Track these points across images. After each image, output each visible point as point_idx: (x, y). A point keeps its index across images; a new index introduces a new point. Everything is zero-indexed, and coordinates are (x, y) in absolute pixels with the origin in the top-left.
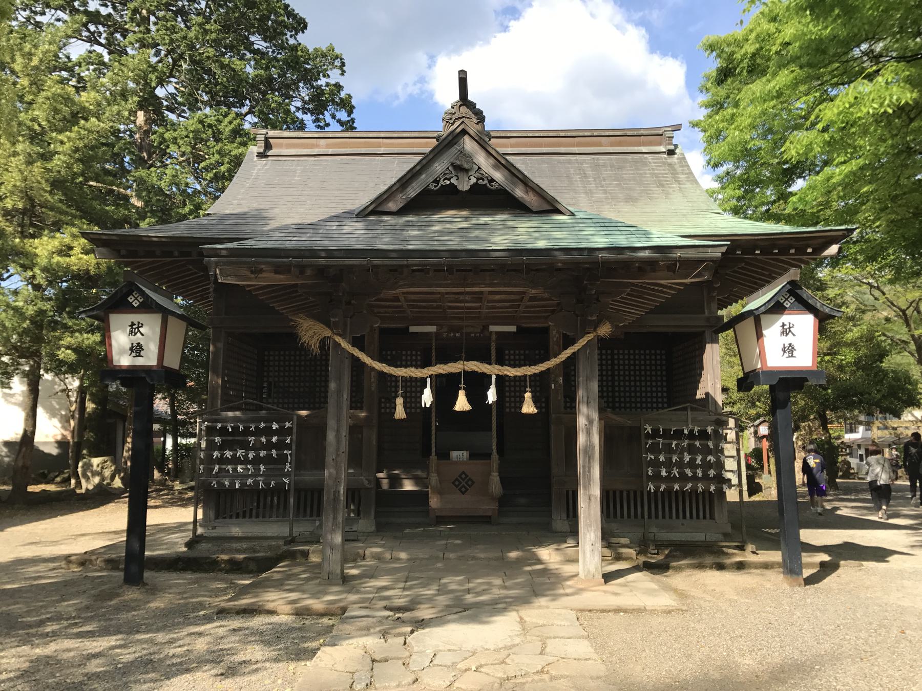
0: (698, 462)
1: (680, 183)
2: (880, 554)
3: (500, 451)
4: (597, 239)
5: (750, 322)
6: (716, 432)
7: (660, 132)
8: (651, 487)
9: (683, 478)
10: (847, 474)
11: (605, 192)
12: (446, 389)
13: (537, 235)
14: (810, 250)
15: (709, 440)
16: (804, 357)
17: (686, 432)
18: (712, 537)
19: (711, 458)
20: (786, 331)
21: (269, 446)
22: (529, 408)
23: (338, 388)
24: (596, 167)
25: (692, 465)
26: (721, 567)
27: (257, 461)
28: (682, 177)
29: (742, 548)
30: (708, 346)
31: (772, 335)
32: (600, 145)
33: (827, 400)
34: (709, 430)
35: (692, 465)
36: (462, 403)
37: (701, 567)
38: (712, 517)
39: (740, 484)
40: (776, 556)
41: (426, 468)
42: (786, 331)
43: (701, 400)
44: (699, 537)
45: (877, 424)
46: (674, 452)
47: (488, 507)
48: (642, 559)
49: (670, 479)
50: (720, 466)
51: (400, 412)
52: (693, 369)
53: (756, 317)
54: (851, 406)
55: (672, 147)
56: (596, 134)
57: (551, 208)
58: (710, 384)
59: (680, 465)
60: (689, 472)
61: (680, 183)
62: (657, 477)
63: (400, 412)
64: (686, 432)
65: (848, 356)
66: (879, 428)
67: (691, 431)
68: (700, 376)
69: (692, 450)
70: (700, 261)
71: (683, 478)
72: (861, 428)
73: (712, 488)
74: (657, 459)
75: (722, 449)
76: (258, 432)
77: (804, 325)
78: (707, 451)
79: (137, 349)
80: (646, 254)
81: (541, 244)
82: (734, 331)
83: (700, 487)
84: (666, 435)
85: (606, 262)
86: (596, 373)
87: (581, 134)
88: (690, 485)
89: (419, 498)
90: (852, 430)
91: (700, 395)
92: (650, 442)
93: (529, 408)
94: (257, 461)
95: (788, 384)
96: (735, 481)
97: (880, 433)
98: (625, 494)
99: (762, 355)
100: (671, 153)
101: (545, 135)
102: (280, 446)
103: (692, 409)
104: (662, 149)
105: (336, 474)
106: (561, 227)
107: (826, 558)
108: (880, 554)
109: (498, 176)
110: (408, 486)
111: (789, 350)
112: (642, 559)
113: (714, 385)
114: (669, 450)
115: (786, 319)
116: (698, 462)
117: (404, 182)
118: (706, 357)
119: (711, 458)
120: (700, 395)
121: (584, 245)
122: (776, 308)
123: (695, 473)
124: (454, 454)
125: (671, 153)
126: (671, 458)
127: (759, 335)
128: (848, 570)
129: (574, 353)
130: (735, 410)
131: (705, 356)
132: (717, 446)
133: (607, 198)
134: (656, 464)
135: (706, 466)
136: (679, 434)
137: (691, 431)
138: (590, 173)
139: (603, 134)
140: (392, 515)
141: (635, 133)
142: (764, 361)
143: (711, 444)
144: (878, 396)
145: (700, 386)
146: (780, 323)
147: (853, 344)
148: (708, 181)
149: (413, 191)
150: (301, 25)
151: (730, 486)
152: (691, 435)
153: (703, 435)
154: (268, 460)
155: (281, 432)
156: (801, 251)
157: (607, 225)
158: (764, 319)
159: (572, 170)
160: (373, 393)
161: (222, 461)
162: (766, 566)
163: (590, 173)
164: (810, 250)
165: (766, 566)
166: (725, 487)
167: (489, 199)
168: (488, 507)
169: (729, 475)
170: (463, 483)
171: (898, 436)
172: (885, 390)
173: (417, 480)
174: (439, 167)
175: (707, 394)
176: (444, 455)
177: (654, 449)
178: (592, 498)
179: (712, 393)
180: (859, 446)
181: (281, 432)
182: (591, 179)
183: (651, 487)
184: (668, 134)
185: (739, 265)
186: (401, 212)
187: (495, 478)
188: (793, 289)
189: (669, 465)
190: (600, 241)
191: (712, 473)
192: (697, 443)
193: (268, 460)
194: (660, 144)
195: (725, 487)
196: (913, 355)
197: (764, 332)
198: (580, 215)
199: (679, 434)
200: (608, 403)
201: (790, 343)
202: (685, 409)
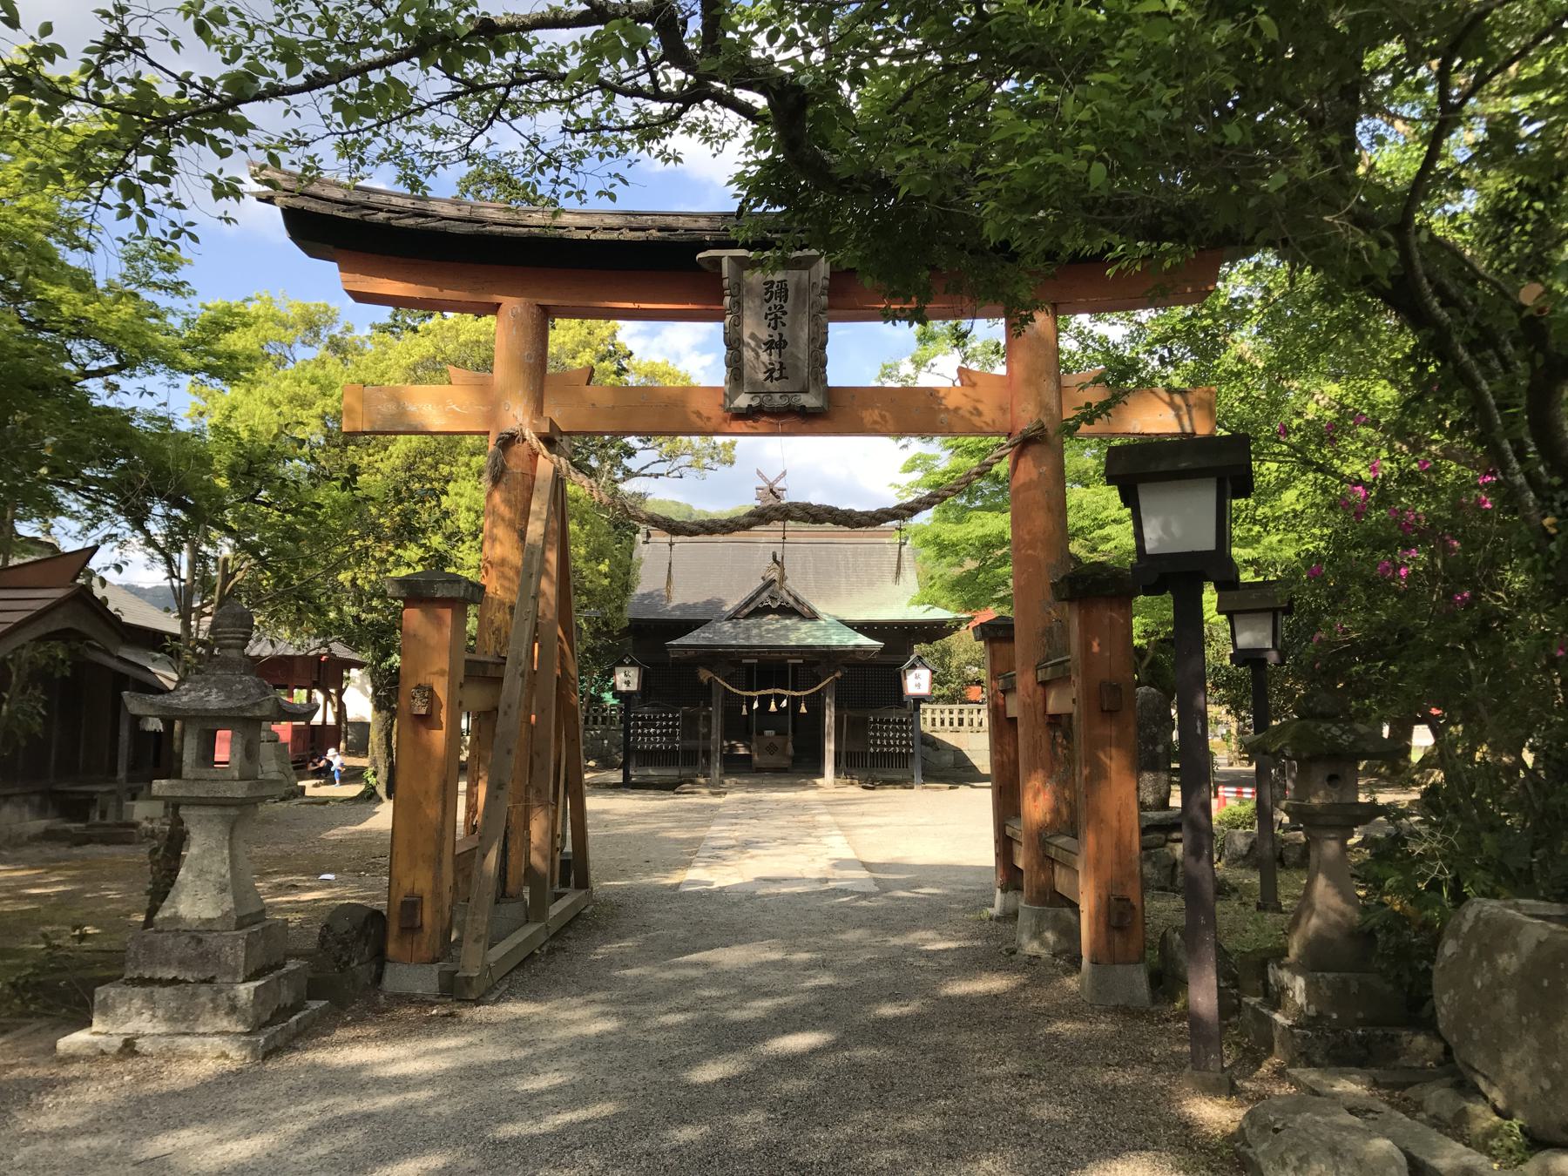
3: (794, 731)
12: (764, 701)
21: (667, 727)
22: (803, 710)
23: (717, 699)
27: (661, 735)
36: (773, 707)
41: (750, 740)
47: (786, 763)
51: (745, 712)
57: (813, 617)
59: (888, 738)
62: (875, 744)
63: (745, 712)
71: (889, 745)
76: (661, 719)
79: (628, 683)
84: (881, 722)
89: (748, 758)
93: (803, 710)
94: (661, 735)
102: (674, 727)
105: (717, 741)
109: (791, 600)
110: (742, 751)
111: (918, 686)
117: (747, 604)
124: (767, 732)
134: (875, 737)
136: (888, 722)
140: (738, 767)
149: (752, 607)
150: (721, 603)
154: (666, 734)
155: (674, 719)
160: (732, 704)
161: (643, 735)
167: (787, 611)
168: (786, 763)
170: (772, 749)
173: (747, 747)
174: (765, 595)
176: (760, 733)
177: (875, 729)
181: (674, 719)
186: (747, 617)
187: (790, 745)
189: (881, 738)
193: (666, 734)
199: (888, 722)
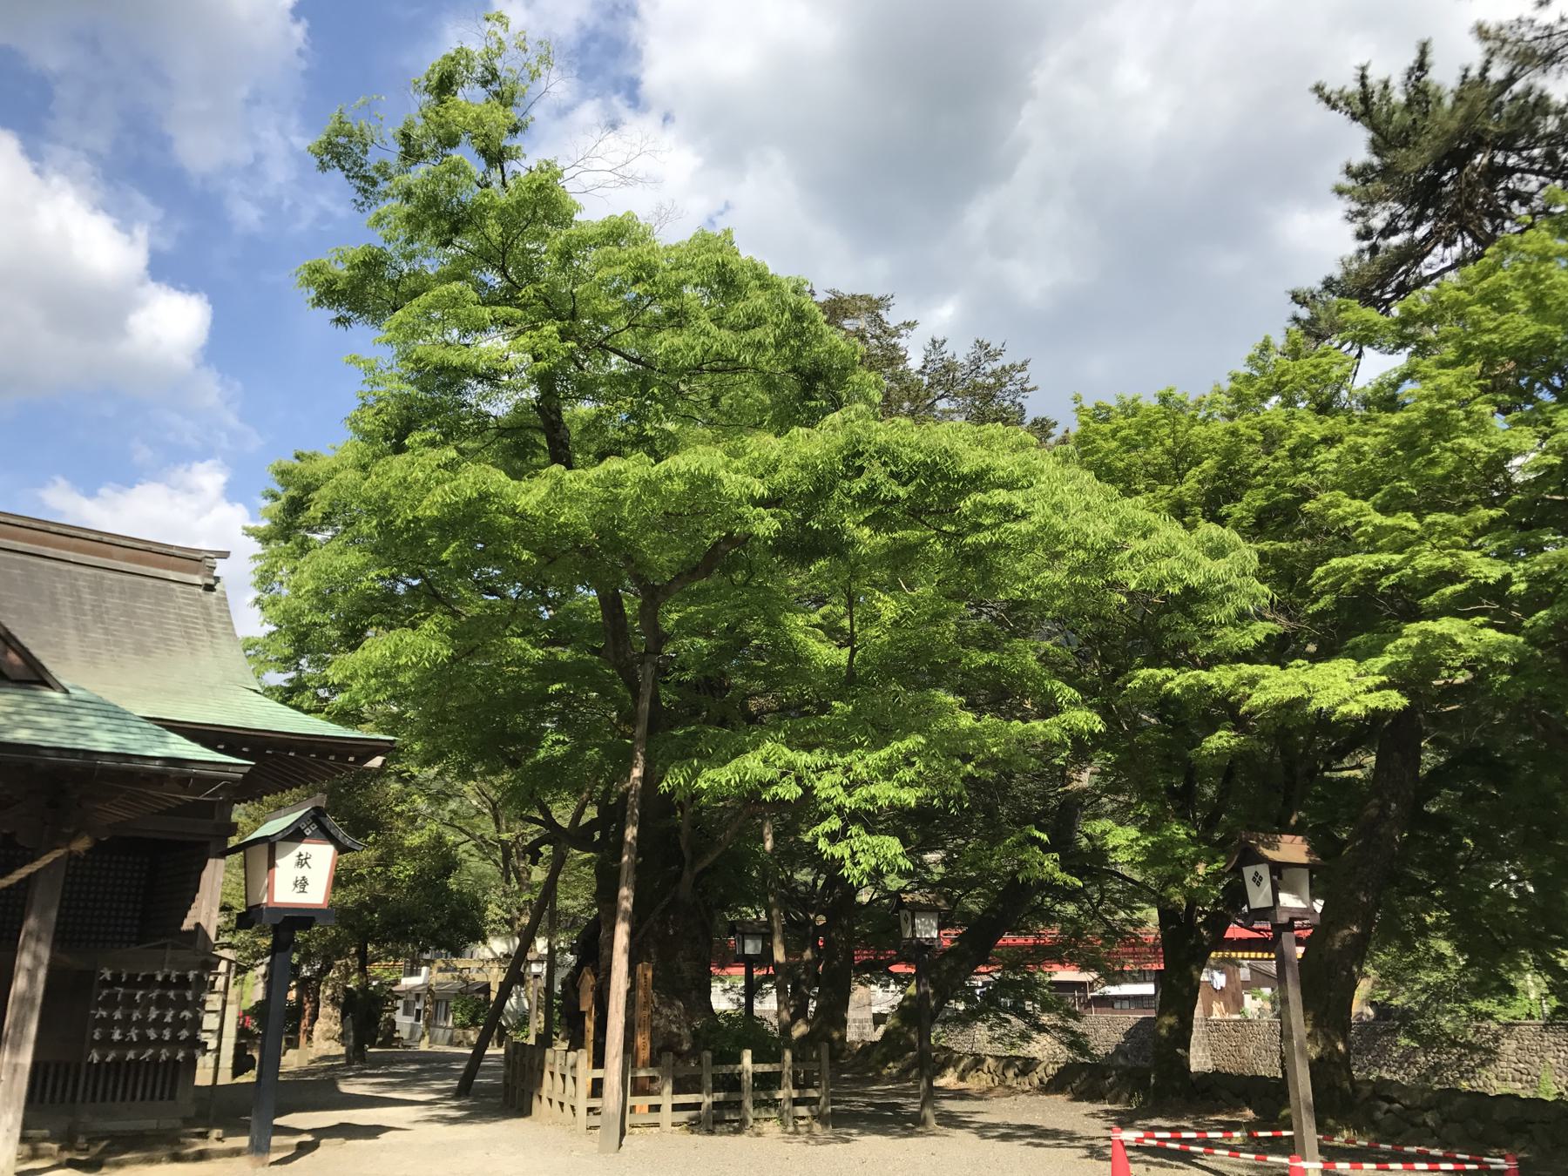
0: (168, 1019)
1: (213, 635)
2: (373, 1131)
4: (97, 734)
5: (264, 847)
6: (199, 978)
7: (199, 556)
8: (95, 1057)
9: (144, 1041)
10: (390, 1038)
11: (106, 631)
13: (16, 718)
14: (351, 759)
15: (189, 990)
16: (316, 895)
17: (159, 978)
18: (166, 1124)
19: (187, 1014)
20: (302, 862)
24: (97, 588)
25: (159, 1024)
26: (177, 1158)
28: (218, 627)
29: (204, 1136)
30: (211, 862)
31: (286, 866)
32: (109, 556)
33: (371, 929)
34: (191, 975)
35: (159, 1024)
37: (150, 1161)
38: (172, 1097)
39: (218, 1049)
40: (243, 1141)
42: (302, 862)
43: (188, 932)
44: (150, 1124)
45: (440, 963)
46: (137, 1006)
48: (67, 1155)
49: (124, 1044)
50: (197, 1023)
52: (188, 890)
53: (271, 846)
54: (402, 937)
55: (212, 581)
56: (106, 539)
58: (203, 913)
59: (143, 1024)
60: (152, 1034)
61: (213, 635)
62: (106, 1042)
64: (159, 978)
65: (404, 870)
66: (440, 970)
67: (167, 977)
68: (193, 900)
69: (162, 1003)
70: (217, 780)
71: (144, 1041)
72: (424, 969)
73: (181, 1055)
74: (111, 1016)
75: (204, 1002)
77: (321, 857)
78: (182, 1004)
80: (156, 766)
81: (23, 735)
82: (245, 856)
83: (164, 1054)
85: (105, 769)
86: (57, 903)
87: (83, 534)
88: (150, 1051)
90: (413, 972)
91: (188, 925)
92: (105, 992)
95: (295, 920)
96: (212, 1044)
97: (440, 977)
98: (52, 1070)
99: (270, 888)
100: (209, 588)
101: (25, 523)
103: (175, 947)
104: (198, 580)
106: (50, 709)
107: (308, 1138)
108: (373, 1131)
112: (67, 1155)
113: (209, 915)
114: (130, 1003)
115: (304, 848)
116: (168, 1019)
118: (206, 875)
119: (187, 1014)
120: (188, 925)
121: (82, 744)
122: (295, 835)
123: (160, 1035)
125: (209, 588)
126: (130, 1016)
127: (272, 865)
128: (328, 1147)
129: (30, 875)
130: (235, 942)
131: (204, 874)
132: (197, 996)
133: (107, 642)
135: (179, 1024)
136: (149, 981)
137: (167, 977)
138: (87, 596)
139: (117, 541)
141: (164, 550)
142: (271, 896)
143: (189, 995)
144: (436, 926)
145: (190, 913)
146: (296, 852)
147: (412, 853)
148: (252, 624)
151: (205, 1051)
152: (166, 983)
153: (183, 982)
156: (342, 757)
157: (113, 714)
158: (280, 847)
159: (59, 586)
162: (236, 1152)
163: (87, 596)
164: (351, 759)
165: (236, 1152)
166: (198, 1052)
169: (203, 1036)
171: (465, 981)
172: (444, 921)
175: (198, 925)
178: (19, 1070)
179: (204, 924)
180: (418, 996)
182: (87, 607)
183: (95, 1057)
184: (209, 562)
185: (272, 762)
188: (317, 816)
189: (126, 1024)
190: (103, 741)
191: (184, 1034)
192: (171, 994)
194: (196, 573)
195: (198, 1052)
196: (497, 864)
197: (278, 862)
198: (76, 693)
199: (149, 981)
200: (62, 940)
201: (305, 877)
202: (164, 946)
